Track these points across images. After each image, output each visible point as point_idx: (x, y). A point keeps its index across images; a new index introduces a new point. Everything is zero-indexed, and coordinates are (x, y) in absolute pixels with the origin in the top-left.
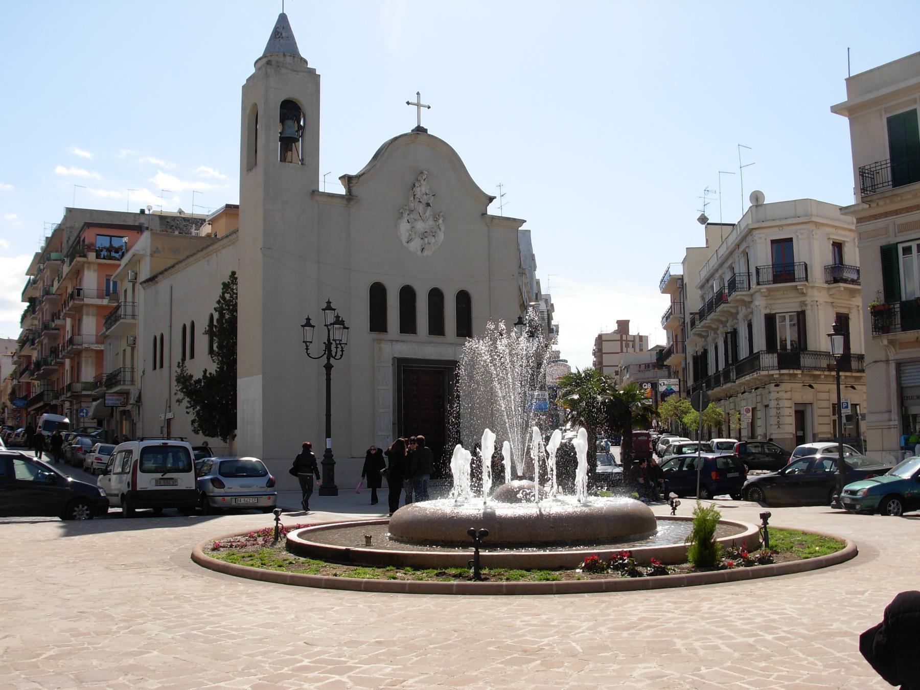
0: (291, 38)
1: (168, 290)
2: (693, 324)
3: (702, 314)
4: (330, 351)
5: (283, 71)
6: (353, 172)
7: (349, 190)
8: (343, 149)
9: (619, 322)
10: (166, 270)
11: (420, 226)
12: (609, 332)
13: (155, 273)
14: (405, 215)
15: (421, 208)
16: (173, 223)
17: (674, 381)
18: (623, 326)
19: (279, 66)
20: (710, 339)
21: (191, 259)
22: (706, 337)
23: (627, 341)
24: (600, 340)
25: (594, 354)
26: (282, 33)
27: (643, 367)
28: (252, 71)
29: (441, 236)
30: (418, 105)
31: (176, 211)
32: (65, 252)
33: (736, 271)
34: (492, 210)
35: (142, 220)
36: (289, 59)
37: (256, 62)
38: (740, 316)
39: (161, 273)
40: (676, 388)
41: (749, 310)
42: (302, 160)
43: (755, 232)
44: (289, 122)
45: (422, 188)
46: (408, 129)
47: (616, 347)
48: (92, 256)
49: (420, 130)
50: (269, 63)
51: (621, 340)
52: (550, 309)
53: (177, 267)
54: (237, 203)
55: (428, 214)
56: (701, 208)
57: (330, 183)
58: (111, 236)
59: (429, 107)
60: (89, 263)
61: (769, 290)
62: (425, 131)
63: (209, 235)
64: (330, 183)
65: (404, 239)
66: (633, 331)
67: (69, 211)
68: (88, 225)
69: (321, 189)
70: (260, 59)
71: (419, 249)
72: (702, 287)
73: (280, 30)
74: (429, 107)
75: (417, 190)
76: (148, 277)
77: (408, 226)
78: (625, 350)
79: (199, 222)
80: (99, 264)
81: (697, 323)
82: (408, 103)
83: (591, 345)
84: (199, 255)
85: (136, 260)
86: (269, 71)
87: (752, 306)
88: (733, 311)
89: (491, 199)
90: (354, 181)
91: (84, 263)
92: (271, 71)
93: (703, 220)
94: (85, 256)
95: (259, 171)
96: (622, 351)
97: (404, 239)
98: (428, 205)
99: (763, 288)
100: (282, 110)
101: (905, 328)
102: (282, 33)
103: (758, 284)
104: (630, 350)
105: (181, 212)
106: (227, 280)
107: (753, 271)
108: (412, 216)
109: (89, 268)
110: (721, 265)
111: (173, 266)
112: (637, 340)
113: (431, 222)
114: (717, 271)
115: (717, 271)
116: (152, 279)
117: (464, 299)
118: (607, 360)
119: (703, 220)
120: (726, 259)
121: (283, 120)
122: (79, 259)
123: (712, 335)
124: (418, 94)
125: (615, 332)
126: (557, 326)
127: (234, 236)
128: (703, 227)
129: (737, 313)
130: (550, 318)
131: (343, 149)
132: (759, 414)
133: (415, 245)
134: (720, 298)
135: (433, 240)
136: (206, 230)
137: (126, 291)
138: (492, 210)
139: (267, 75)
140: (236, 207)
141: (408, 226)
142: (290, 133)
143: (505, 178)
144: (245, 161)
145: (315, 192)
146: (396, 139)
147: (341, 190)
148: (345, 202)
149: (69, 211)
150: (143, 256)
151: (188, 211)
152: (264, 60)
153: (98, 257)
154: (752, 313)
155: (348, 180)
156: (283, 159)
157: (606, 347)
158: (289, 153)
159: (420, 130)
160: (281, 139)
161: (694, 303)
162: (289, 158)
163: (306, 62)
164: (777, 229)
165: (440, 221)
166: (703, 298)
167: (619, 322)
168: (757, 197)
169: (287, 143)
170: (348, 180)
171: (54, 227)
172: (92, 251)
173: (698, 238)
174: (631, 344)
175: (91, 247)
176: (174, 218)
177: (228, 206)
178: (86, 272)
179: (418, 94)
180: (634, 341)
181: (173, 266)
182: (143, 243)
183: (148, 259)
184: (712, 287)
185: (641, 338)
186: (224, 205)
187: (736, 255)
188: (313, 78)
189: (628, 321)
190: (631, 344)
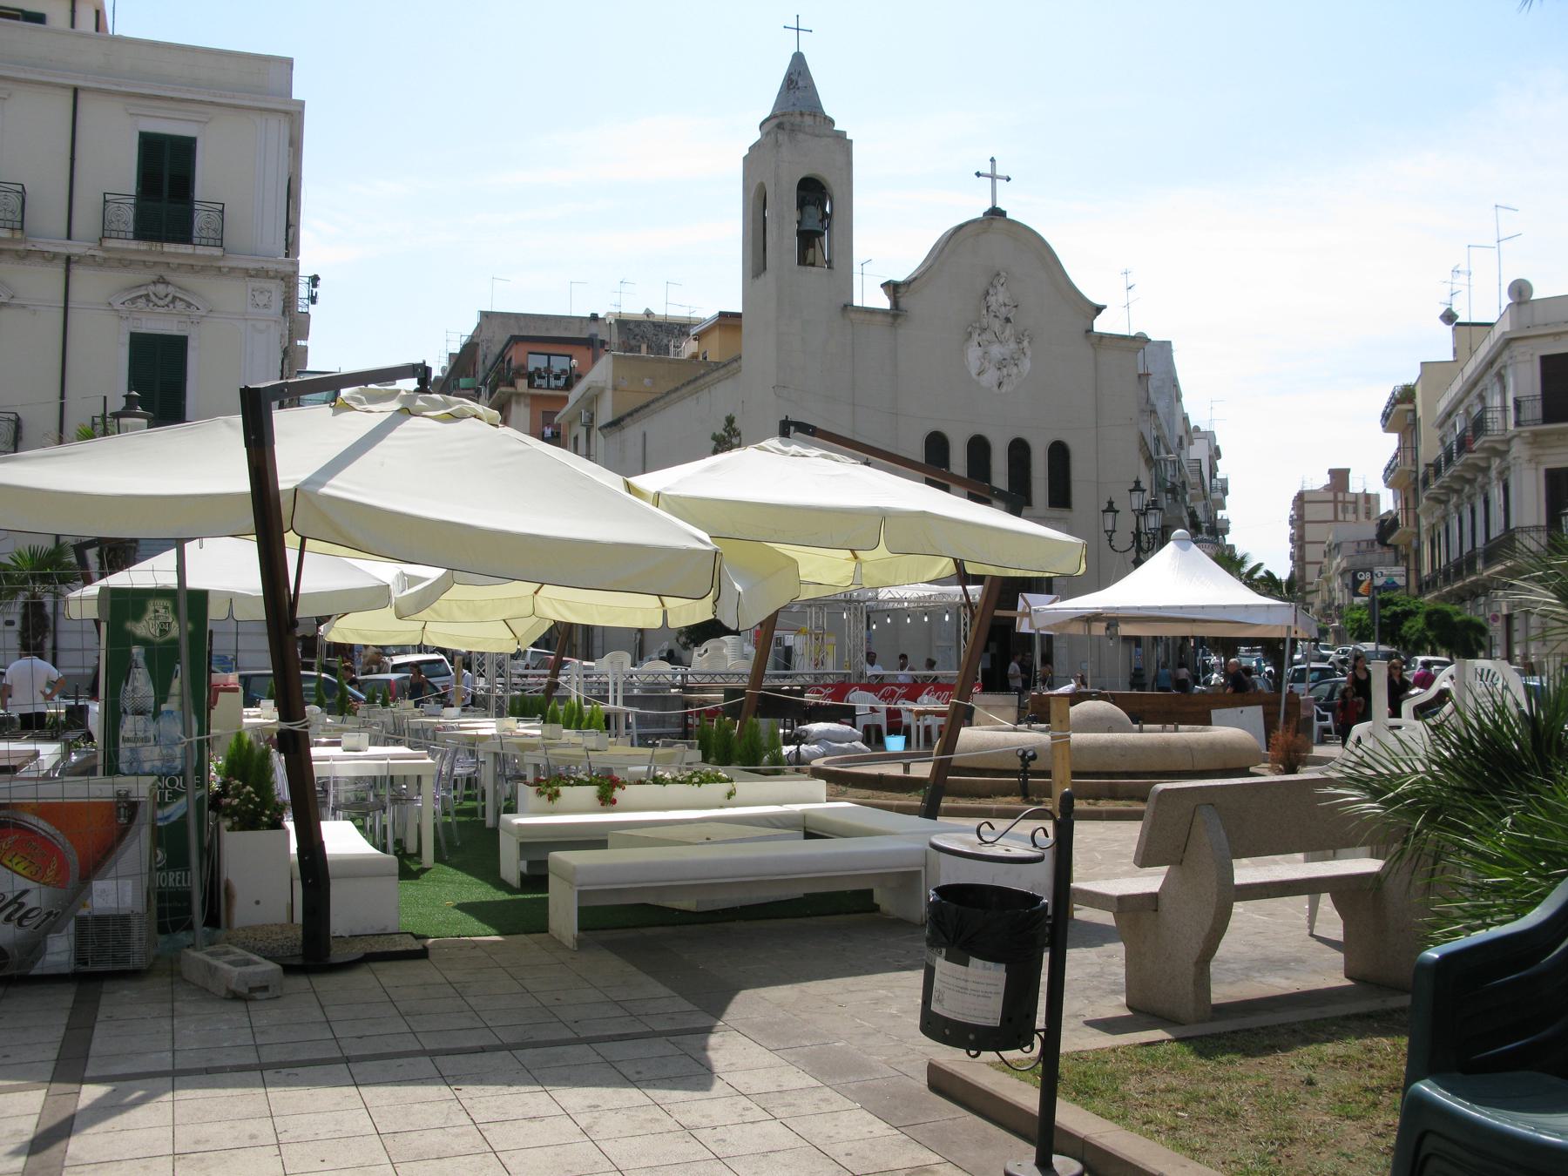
0: (810, 87)
1: (640, 439)
2: (1426, 483)
3: (1436, 468)
4: (1139, 542)
5: (801, 136)
6: (900, 277)
7: (895, 303)
8: (886, 244)
9: (1333, 472)
10: (637, 411)
11: (996, 351)
12: (1316, 487)
13: (618, 415)
14: (975, 336)
15: (997, 325)
16: (637, 331)
17: (1401, 569)
18: (1340, 477)
19: (794, 130)
20: (1451, 506)
21: (674, 396)
22: (1446, 502)
23: (1344, 502)
24: (1301, 500)
25: (1291, 523)
26: (798, 80)
27: (1363, 546)
28: (756, 136)
29: (1026, 365)
30: (993, 177)
31: (641, 311)
32: (480, 376)
33: (1489, 403)
34: (1101, 325)
35: (594, 329)
36: (808, 120)
37: (763, 124)
38: (1493, 473)
39: (630, 414)
40: (1401, 581)
41: (1504, 464)
42: (829, 262)
43: (1514, 345)
44: (811, 210)
45: (999, 297)
46: (977, 210)
47: (1327, 512)
48: (522, 385)
49: (995, 213)
50: (780, 126)
51: (1335, 501)
52: (1216, 453)
53: (653, 407)
54: (739, 309)
55: (1007, 332)
56: (1447, 299)
57: (869, 294)
58: (549, 355)
59: (1008, 179)
60: (519, 395)
61: (1535, 434)
62: (1003, 214)
63: (694, 356)
64: (869, 294)
65: (974, 372)
66: (1355, 486)
67: (486, 316)
68: (515, 340)
69: (857, 302)
70: (767, 120)
71: (995, 384)
72: (1441, 426)
73: (794, 77)
74: (978, 174)
75: (992, 299)
76: (610, 419)
77: (979, 352)
78: (1341, 517)
79: (679, 329)
80: (534, 397)
81: (1432, 480)
82: (978, 174)
83: (1286, 510)
84: (684, 391)
85: (592, 399)
86: (780, 137)
87: (1510, 458)
88: (1483, 464)
89: (1099, 310)
90: (902, 290)
91: (510, 396)
92: (783, 137)
93: (1449, 317)
94: (512, 384)
95: (769, 276)
96: (1336, 520)
97: (974, 372)
98: (1008, 320)
99: (1526, 430)
100: (800, 191)
101: (1015, 608)
102: (798, 80)
103: (1518, 423)
104: (1350, 517)
105: (648, 313)
106: (720, 431)
107: (1510, 403)
108: (984, 337)
109: (518, 403)
110: (1468, 392)
111: (647, 405)
112: (1362, 501)
113: (1012, 345)
114: (1461, 401)
115: (1461, 401)
116: (616, 424)
117: (1059, 454)
118: (1311, 532)
119: (1449, 317)
120: (1475, 384)
121: (801, 204)
122: (503, 389)
123: (1454, 499)
124: (992, 160)
125: (1326, 488)
126: (1225, 481)
127: (735, 365)
128: (1448, 330)
129: (1489, 468)
130: (1213, 470)
131: (886, 244)
132: (1517, 624)
133: (991, 377)
134: (1463, 444)
135: (1015, 370)
136: (689, 348)
137: (576, 438)
138: (1101, 325)
139: (777, 144)
140: (737, 316)
141: (979, 352)
142: (812, 224)
143: (1125, 273)
144: (750, 264)
145: (848, 307)
146: (961, 227)
147: (883, 302)
148: (890, 319)
149: (486, 316)
150: (602, 390)
151: (660, 311)
152: (775, 122)
153: (530, 385)
154: (1508, 468)
155: (892, 288)
156: (803, 260)
157: (1311, 512)
158: (811, 251)
159: (995, 213)
160: (800, 233)
161: (1430, 449)
162: (810, 258)
163: (832, 122)
164: (1550, 339)
165: (1025, 343)
166: (1442, 440)
167: (1333, 472)
168: (1520, 291)
169: (807, 239)
170: (892, 288)
171: (464, 339)
172: (522, 376)
173: (1442, 346)
174: (1351, 507)
175: (521, 372)
176: (638, 323)
177: (722, 315)
178: (514, 407)
179: (992, 160)
180: (1356, 503)
181: (647, 405)
182: (601, 372)
183: (609, 394)
184: (1454, 425)
185: (1367, 497)
186: (715, 312)
187: (1486, 380)
188: (843, 144)
189: (1347, 471)
190: (1351, 507)
